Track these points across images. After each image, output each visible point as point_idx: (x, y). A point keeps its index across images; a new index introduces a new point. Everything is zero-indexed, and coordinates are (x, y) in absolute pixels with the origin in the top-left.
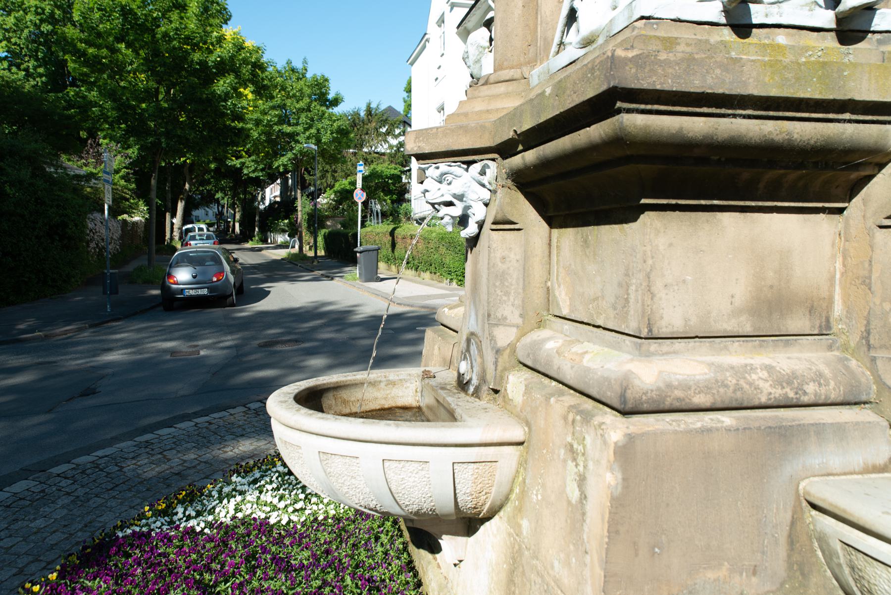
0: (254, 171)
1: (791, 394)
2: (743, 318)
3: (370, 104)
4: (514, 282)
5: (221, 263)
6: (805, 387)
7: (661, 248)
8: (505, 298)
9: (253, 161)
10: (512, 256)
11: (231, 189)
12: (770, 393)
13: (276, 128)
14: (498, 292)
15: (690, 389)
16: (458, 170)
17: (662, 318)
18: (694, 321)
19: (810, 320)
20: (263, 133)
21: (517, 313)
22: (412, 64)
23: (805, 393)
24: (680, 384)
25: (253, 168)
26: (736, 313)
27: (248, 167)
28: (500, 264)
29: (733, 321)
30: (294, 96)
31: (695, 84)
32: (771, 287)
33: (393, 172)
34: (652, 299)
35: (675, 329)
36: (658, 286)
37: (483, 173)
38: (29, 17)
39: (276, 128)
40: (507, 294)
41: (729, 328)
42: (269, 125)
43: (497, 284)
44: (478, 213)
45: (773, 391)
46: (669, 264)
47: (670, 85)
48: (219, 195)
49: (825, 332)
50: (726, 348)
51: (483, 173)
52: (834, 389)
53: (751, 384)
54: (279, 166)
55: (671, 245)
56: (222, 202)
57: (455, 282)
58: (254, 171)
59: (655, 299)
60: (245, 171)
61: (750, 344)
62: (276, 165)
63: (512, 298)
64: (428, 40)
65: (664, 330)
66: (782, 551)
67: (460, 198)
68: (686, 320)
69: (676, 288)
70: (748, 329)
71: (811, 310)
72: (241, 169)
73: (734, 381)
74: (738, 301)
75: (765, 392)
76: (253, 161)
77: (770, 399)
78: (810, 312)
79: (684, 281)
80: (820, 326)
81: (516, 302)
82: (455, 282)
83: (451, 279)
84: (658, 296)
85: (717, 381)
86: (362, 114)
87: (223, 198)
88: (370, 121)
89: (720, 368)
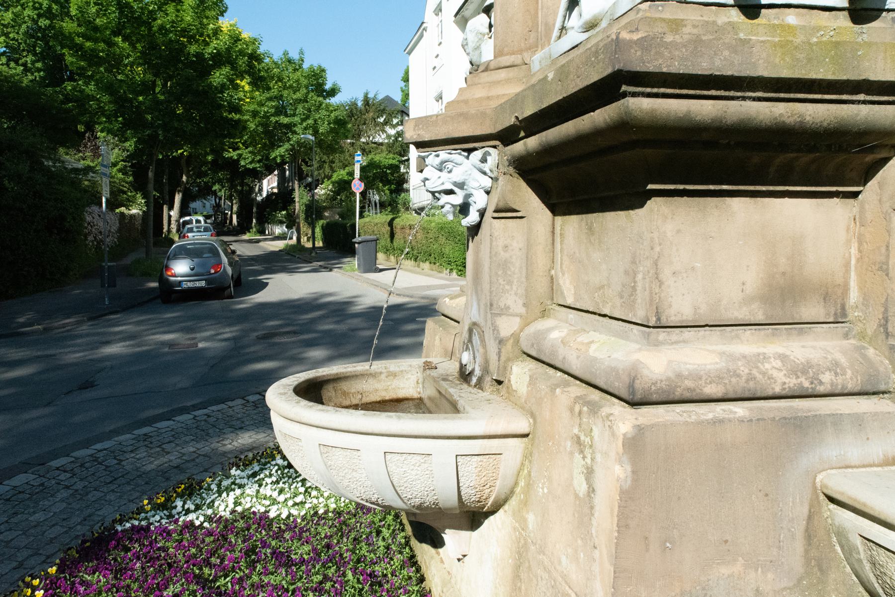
0: (251, 163)
1: (806, 384)
2: (755, 306)
3: (367, 94)
4: (517, 271)
5: (218, 255)
6: (821, 377)
7: (669, 234)
8: (507, 287)
9: (250, 152)
10: (515, 244)
11: (228, 180)
12: (785, 383)
13: (273, 119)
14: (501, 281)
15: (700, 379)
16: (458, 157)
17: (670, 306)
18: (703, 309)
19: (825, 307)
20: (260, 124)
21: (520, 302)
22: (409, 53)
23: (821, 383)
24: (690, 374)
25: (250, 159)
26: (748, 300)
27: (245, 159)
28: (502, 253)
29: (745, 309)
30: (291, 87)
31: (703, 67)
32: (784, 274)
33: (391, 162)
34: (660, 287)
35: (685, 318)
36: (666, 273)
37: (484, 160)
38: (27, 12)
39: (273, 119)
40: (510, 283)
41: (740, 317)
42: (266, 116)
43: (500, 273)
44: (479, 200)
45: (787, 381)
46: (677, 250)
47: (677, 67)
48: (216, 187)
49: (840, 320)
50: (737, 336)
51: (484, 160)
52: (851, 379)
53: (764, 374)
54: (276, 157)
55: (679, 231)
56: (219, 194)
57: (455, 271)
58: (251, 163)
59: (663, 287)
60: (242, 163)
61: (763, 332)
62: (273, 155)
63: (514, 288)
64: (425, 29)
65: (673, 318)
66: (799, 546)
67: (461, 186)
68: (696, 309)
69: (685, 275)
70: (760, 318)
71: (826, 297)
72: (238, 161)
73: (747, 371)
74: (750, 289)
75: (779, 381)
76: (250, 152)
77: (784, 389)
78: (824, 299)
79: (693, 268)
80: (835, 314)
81: (519, 291)
82: (455, 271)
83: (451, 270)
84: (666, 283)
85: (729, 371)
86: (360, 104)
87: (220, 190)
88: (367, 112)
89: (732, 357)
